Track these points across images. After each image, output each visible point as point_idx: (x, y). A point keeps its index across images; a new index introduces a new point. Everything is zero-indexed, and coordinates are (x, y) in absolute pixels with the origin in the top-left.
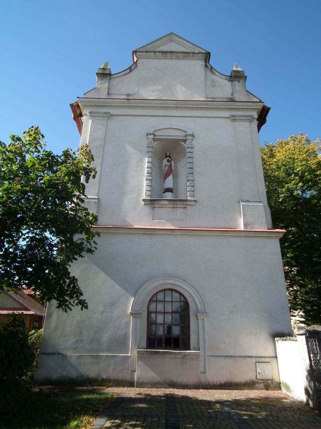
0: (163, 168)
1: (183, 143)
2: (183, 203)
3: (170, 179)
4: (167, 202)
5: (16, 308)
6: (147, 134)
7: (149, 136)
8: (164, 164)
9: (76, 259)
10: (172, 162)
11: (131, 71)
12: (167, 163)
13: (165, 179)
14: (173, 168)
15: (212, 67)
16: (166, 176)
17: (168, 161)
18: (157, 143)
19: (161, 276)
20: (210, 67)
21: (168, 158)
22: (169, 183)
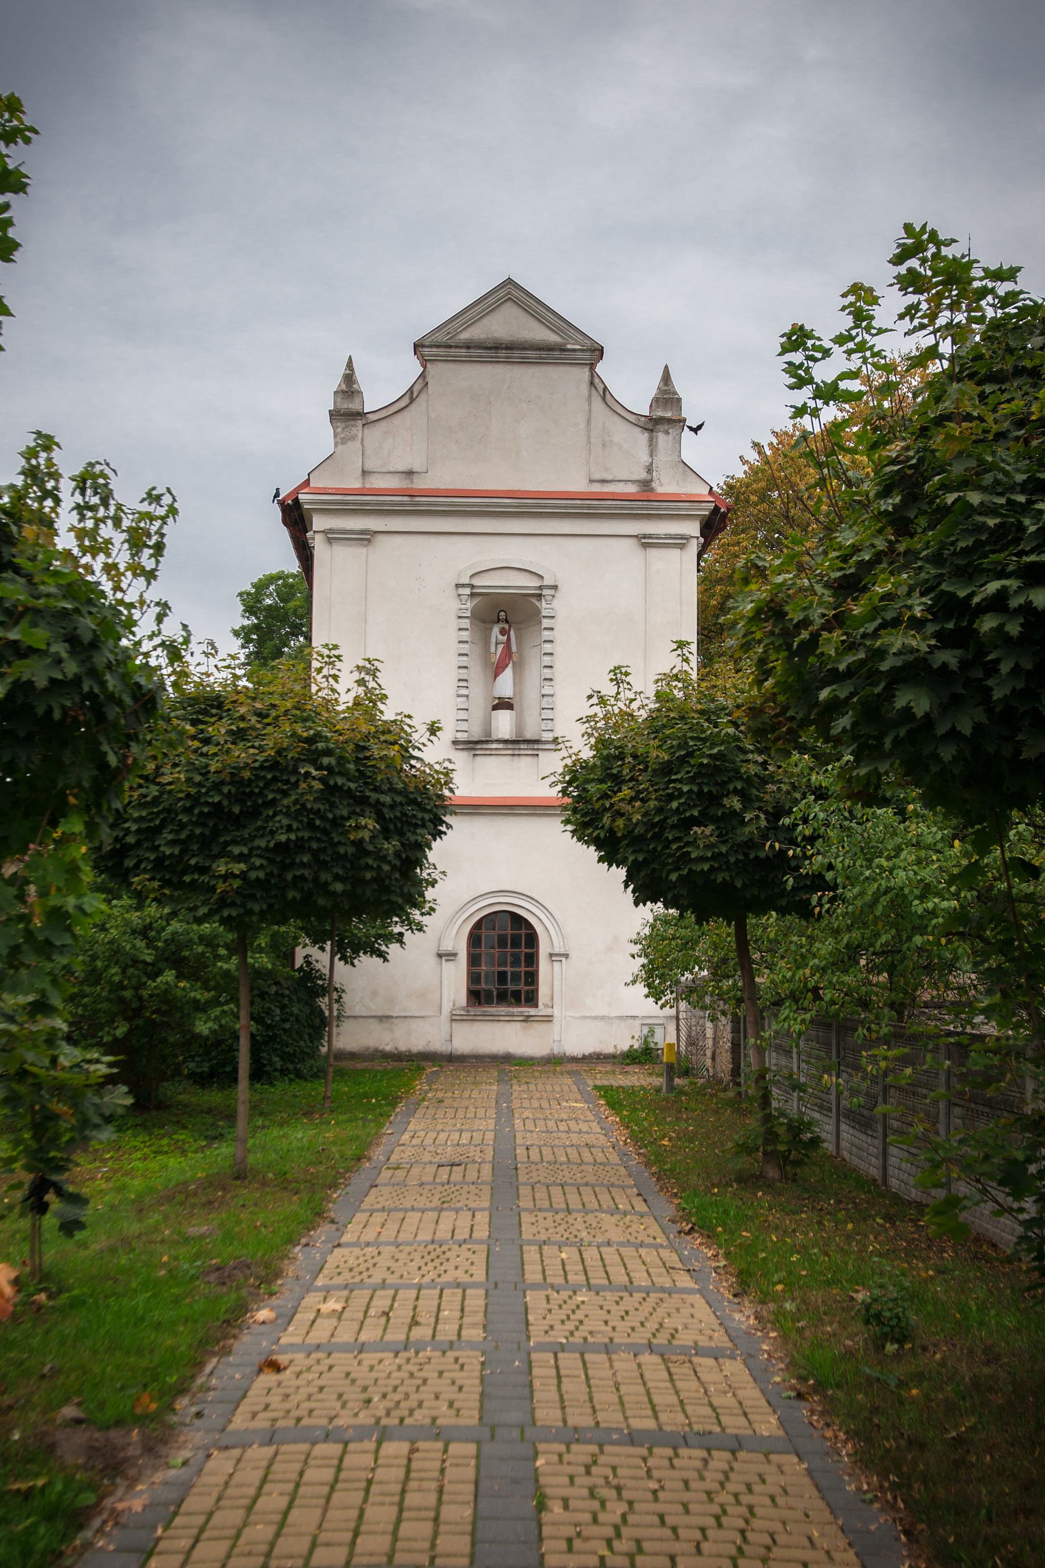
0: (493, 650)
1: (534, 600)
2: (531, 746)
3: (507, 675)
4: (501, 746)
5: (732, 1070)
6: (458, 586)
7: (461, 591)
8: (493, 640)
9: (399, 938)
10: (512, 633)
11: (412, 400)
12: (500, 637)
13: (496, 675)
14: (514, 648)
15: (605, 389)
16: (498, 670)
17: (503, 632)
18: (476, 600)
19: (322, 1462)
20: (600, 387)
21: (501, 625)
22: (505, 685)
